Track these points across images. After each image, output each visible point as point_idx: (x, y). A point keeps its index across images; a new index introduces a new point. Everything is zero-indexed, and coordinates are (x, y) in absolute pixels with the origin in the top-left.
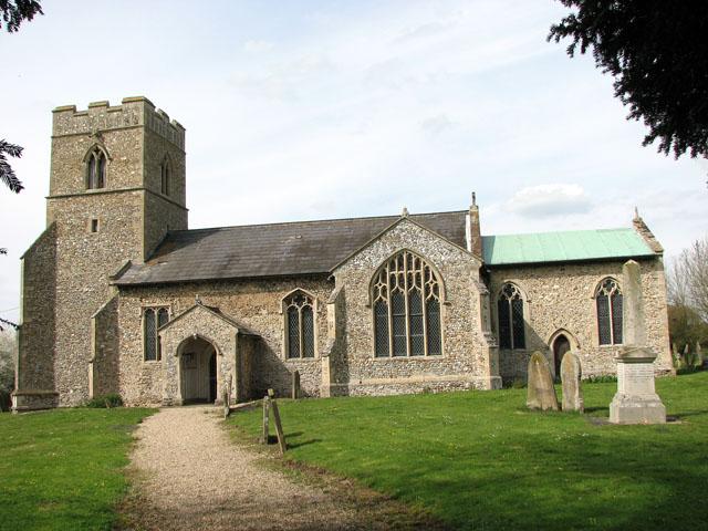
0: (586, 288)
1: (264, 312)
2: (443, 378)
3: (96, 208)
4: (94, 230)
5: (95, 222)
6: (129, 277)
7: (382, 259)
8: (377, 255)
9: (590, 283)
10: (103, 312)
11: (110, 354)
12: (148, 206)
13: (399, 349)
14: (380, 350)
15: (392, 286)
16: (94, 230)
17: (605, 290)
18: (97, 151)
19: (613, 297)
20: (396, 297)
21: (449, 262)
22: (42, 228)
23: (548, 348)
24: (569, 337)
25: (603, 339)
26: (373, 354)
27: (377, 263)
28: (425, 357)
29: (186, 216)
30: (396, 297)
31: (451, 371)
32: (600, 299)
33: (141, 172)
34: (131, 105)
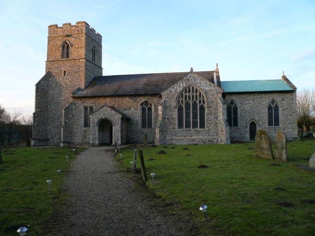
0: (264, 103)
1: (132, 109)
2: (206, 137)
3: (66, 66)
4: (65, 75)
5: (65, 72)
6: (80, 93)
7: (182, 88)
8: (179, 87)
9: (266, 101)
10: (67, 108)
11: (70, 124)
12: (86, 65)
13: (188, 126)
14: (180, 126)
15: (186, 100)
16: (65, 75)
17: (271, 104)
18: (66, 43)
19: (275, 107)
20: (187, 104)
21: (209, 90)
22: (42, 73)
23: (246, 127)
24: (256, 122)
25: (270, 124)
26: (177, 127)
27: (179, 89)
28: (199, 129)
29: (102, 71)
30: (187, 104)
31: (209, 135)
32: (270, 108)
33: (84, 52)
34: (80, 25)
